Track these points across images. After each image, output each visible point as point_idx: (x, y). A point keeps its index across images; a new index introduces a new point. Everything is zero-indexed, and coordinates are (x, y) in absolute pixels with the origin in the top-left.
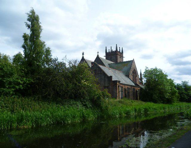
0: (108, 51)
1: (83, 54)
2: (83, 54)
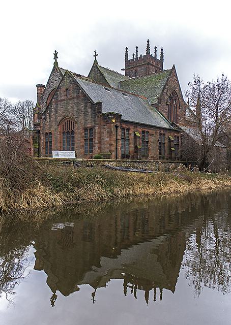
0: (130, 58)
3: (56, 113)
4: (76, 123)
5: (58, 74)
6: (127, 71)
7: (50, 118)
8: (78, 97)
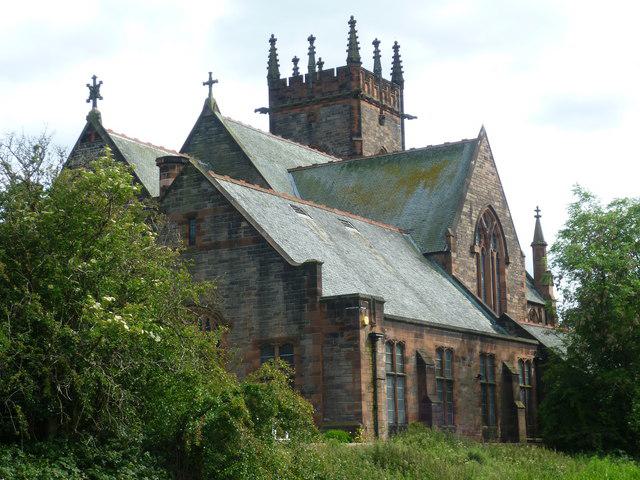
1: (94, 93)
2: (94, 93)
6: (280, 116)
8: (231, 244)
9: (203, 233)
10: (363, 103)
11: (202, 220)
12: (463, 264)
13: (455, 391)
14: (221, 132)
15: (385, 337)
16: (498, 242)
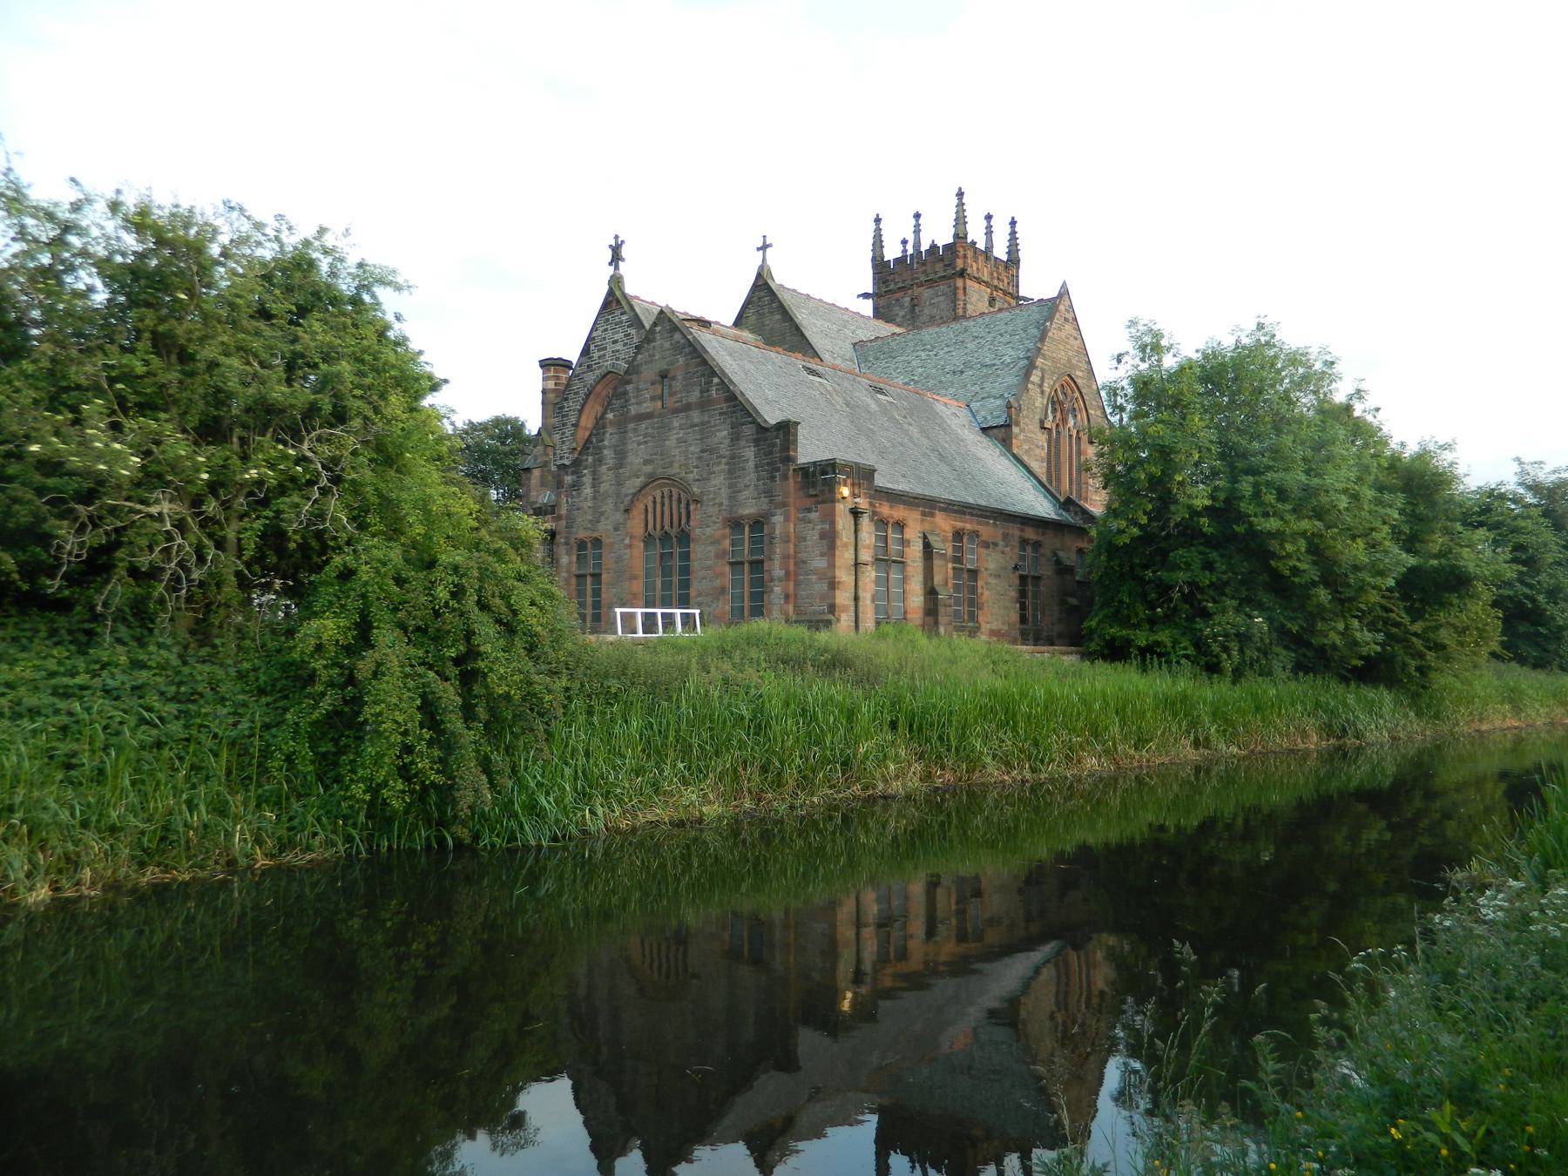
0: (892, 252)
1: (616, 257)
2: (616, 257)
3: (620, 465)
4: (696, 502)
5: (624, 318)
6: (882, 302)
7: (596, 483)
8: (704, 405)
9: (676, 393)
10: (969, 282)
11: (673, 378)
12: (1029, 440)
13: (980, 583)
14: (772, 301)
15: (874, 513)
16: (1079, 417)
